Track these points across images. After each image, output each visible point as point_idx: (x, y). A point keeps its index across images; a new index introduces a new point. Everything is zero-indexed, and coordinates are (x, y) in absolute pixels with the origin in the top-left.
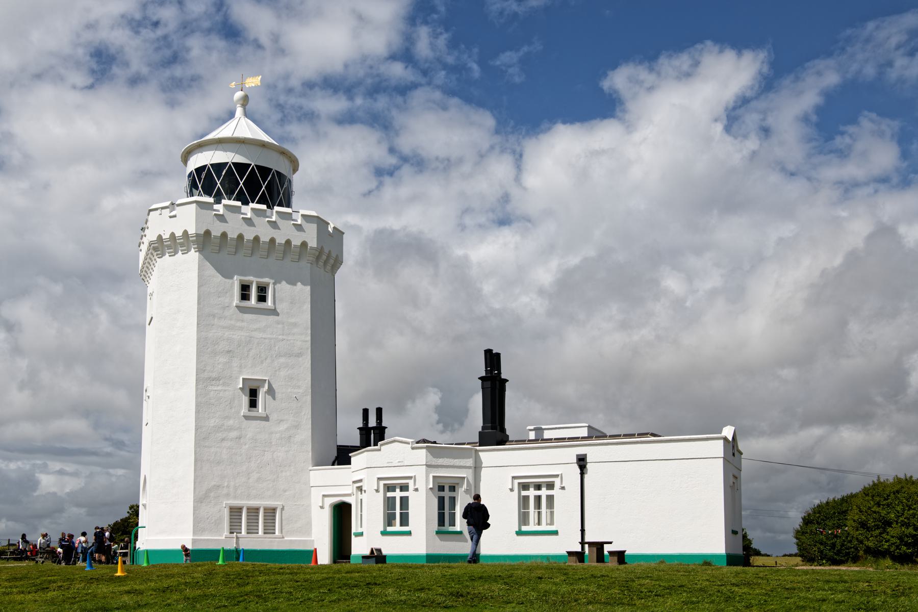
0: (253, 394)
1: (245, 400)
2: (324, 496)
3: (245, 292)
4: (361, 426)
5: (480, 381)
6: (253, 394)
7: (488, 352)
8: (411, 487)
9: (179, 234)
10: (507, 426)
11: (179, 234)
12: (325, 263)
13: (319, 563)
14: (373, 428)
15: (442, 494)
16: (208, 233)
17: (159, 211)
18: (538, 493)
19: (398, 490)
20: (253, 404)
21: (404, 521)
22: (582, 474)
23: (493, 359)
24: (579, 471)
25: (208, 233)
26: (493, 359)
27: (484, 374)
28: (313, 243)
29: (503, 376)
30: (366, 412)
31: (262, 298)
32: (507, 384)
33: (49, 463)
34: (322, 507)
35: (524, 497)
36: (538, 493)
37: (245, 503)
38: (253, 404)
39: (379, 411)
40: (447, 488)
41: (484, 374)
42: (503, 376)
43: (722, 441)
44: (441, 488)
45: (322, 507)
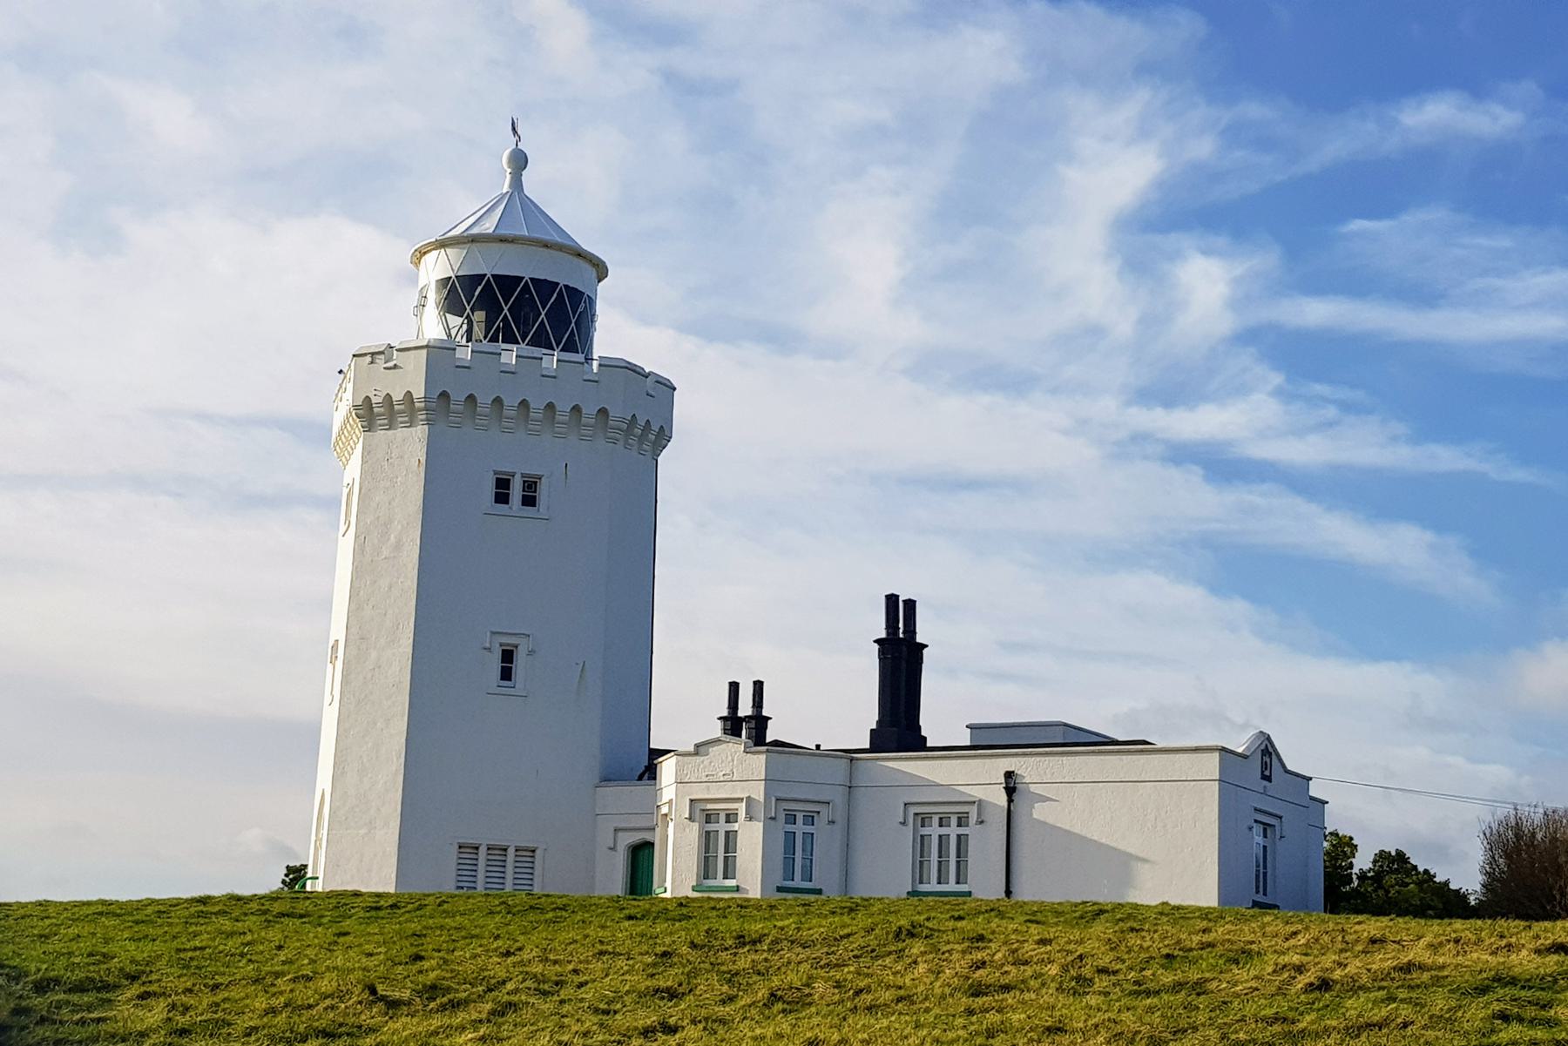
0: (508, 656)
1: (497, 656)
2: (616, 830)
3: (503, 485)
4: (725, 713)
5: (876, 646)
6: (508, 656)
9: (398, 396)
11: (398, 396)
13: (1214, 903)
15: (790, 828)
16: (444, 395)
17: (368, 359)
18: (944, 831)
20: (506, 674)
22: (1010, 801)
23: (900, 612)
25: (444, 395)
26: (900, 612)
27: (883, 635)
28: (419, 392)
29: (919, 639)
30: (734, 687)
31: (529, 501)
34: (904, 823)
36: (944, 831)
37: (484, 837)
38: (506, 674)
39: (758, 686)
41: (883, 635)
42: (919, 639)
43: (1216, 755)
44: (791, 818)
45: (613, 849)
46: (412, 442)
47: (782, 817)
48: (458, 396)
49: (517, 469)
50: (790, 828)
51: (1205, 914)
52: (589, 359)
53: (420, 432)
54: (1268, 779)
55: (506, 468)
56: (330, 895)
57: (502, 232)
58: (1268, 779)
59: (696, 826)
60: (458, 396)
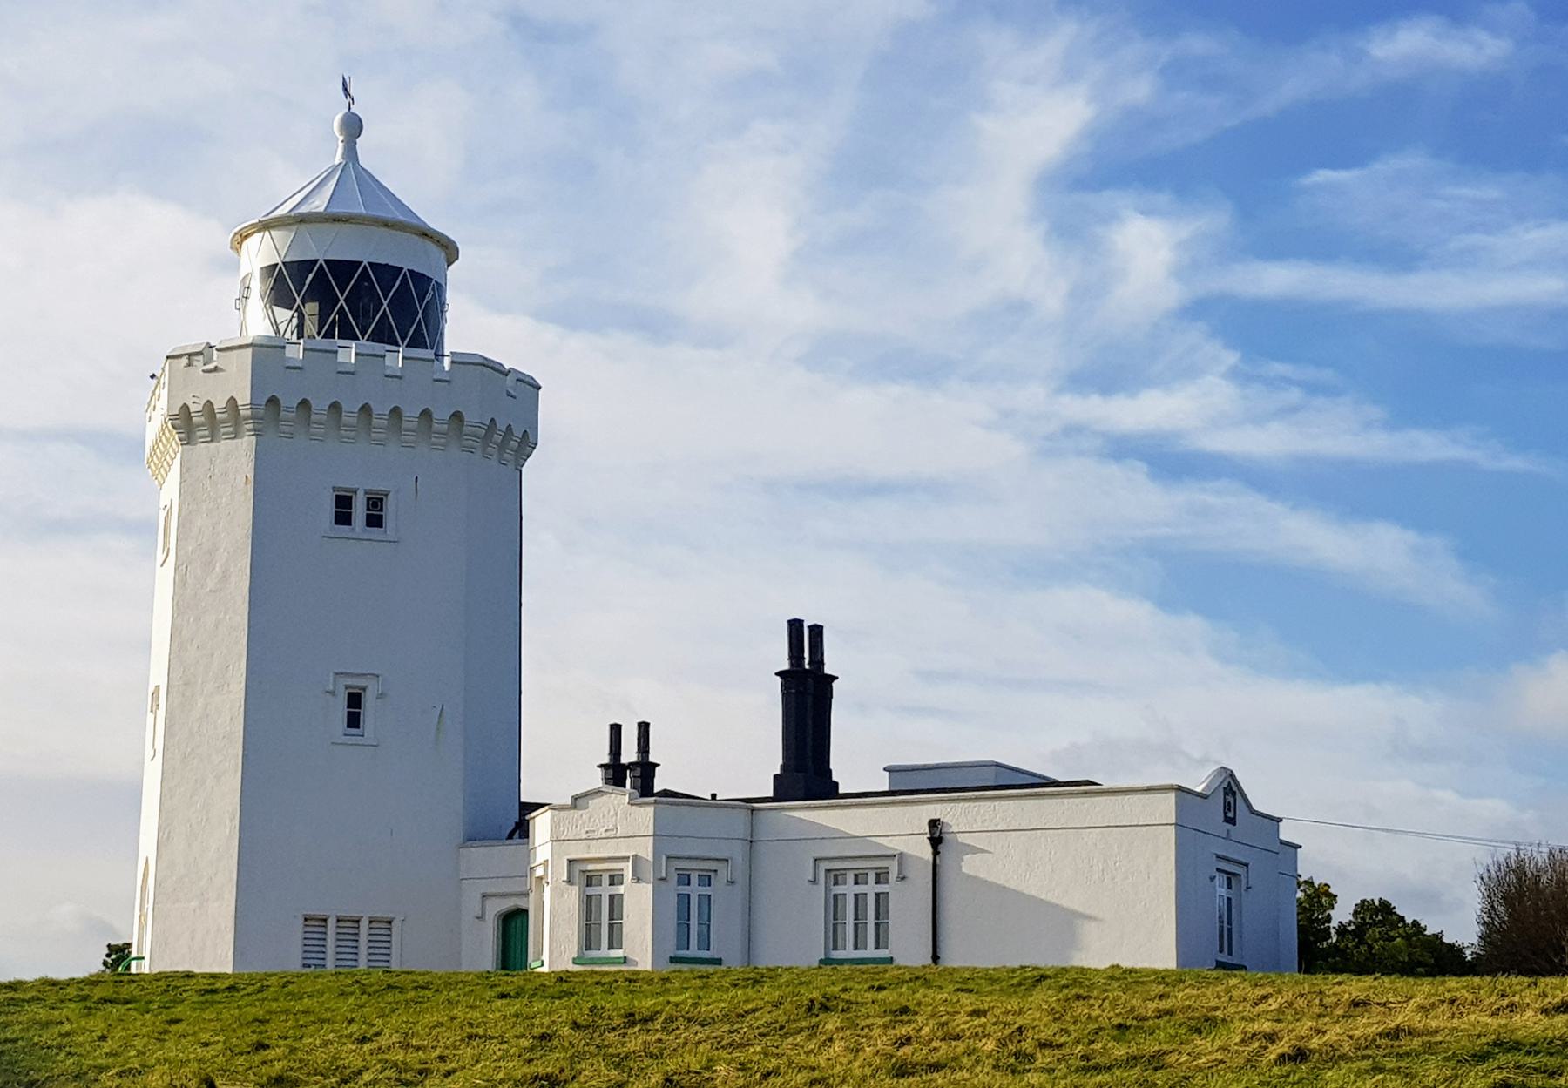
0: (354, 700)
2: (484, 896)
3: (344, 503)
5: (779, 680)
6: (354, 700)
7: (795, 626)
9: (220, 403)
11: (220, 403)
12: (502, 446)
14: (631, 766)
15: (684, 889)
16: (273, 401)
17: (185, 360)
18: (860, 889)
20: (354, 721)
21: (705, 943)
22: (936, 853)
24: (930, 850)
25: (273, 401)
28: (244, 399)
29: (827, 671)
30: (616, 730)
31: (375, 521)
32: (835, 684)
33: (539, 860)
35: (835, 896)
36: (860, 889)
38: (354, 721)
39: (644, 728)
40: (694, 879)
41: (786, 666)
42: (827, 671)
44: (684, 879)
46: (237, 456)
48: (289, 402)
49: (361, 484)
50: (684, 889)
53: (247, 443)
54: (1232, 821)
55: (346, 484)
57: (337, 210)
58: (1232, 821)
60: (289, 402)
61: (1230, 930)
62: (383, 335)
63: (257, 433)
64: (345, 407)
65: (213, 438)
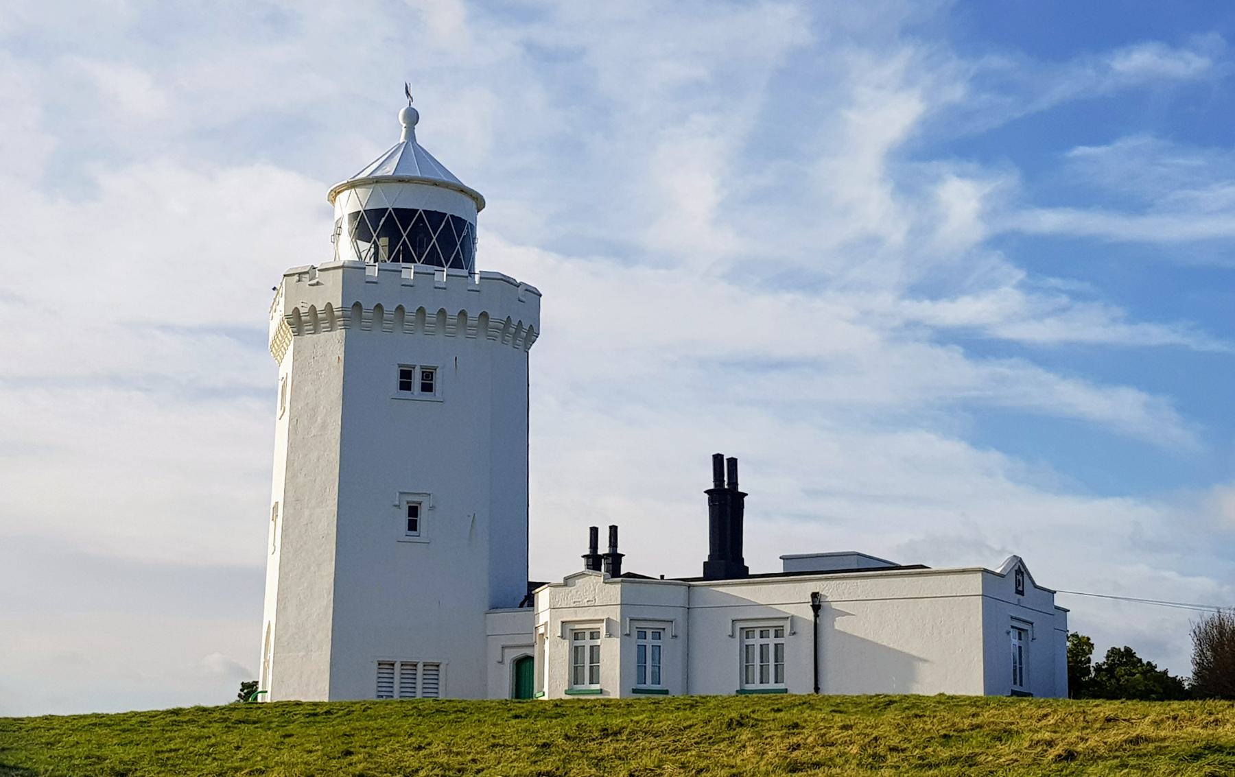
0: (413, 511)
3: (406, 375)
5: (707, 496)
6: (413, 511)
8: (787, 630)
9: (320, 307)
10: (746, 554)
11: (320, 307)
15: (642, 642)
16: (357, 305)
18: (764, 641)
19: (749, 642)
20: (413, 526)
22: (816, 616)
23: (724, 468)
26: (724, 468)
28: (337, 303)
29: (740, 490)
30: (594, 532)
31: (427, 387)
32: (746, 499)
36: (764, 641)
37: (421, 660)
38: (413, 526)
39: (614, 530)
42: (740, 490)
44: (642, 634)
45: (501, 662)
47: (635, 634)
49: (417, 362)
50: (642, 642)
51: (974, 702)
52: (472, 273)
53: (339, 334)
54: (1021, 593)
56: (277, 705)
57: (401, 174)
58: (1021, 593)
59: (566, 642)
60: (369, 305)
61: (1021, 669)
62: (433, 260)
63: (346, 327)
64: (302, 310)
65: (316, 331)
